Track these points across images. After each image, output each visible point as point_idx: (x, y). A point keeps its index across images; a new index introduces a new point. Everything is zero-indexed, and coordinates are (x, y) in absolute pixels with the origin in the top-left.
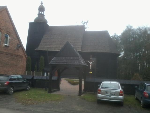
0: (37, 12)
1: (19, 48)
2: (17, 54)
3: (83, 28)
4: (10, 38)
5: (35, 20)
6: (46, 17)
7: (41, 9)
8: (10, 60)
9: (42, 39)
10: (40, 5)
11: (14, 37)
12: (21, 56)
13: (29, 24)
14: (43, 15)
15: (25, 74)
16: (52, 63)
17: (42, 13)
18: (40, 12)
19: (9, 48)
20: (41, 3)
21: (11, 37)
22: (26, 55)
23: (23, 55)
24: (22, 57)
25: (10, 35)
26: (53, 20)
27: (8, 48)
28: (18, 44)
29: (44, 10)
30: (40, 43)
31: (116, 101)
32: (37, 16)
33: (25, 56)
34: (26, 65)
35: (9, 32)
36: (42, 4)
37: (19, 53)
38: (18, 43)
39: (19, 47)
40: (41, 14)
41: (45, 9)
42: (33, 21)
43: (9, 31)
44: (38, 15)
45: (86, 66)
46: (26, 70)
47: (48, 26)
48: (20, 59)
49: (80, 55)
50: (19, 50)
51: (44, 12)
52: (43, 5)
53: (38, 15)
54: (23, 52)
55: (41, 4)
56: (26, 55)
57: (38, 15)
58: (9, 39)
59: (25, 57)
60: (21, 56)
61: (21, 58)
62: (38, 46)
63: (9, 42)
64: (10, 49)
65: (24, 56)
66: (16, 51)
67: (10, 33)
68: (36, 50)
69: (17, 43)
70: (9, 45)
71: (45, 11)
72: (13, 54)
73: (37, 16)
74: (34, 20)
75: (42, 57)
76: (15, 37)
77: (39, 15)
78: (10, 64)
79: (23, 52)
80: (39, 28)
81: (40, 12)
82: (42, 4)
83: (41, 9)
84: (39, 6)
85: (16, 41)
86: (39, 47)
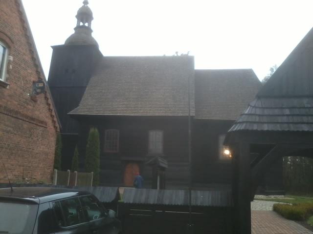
0: (74, 23)
1: (38, 94)
2: (29, 114)
4: (11, 58)
6: (94, 35)
7: (85, 15)
8: (8, 132)
9: (86, 87)
10: (81, 5)
11: (24, 56)
12: (42, 122)
13: (51, 50)
14: (88, 30)
15: (52, 178)
17: (86, 24)
18: (81, 24)
19: (7, 91)
21: (13, 55)
22: (55, 119)
23: (47, 120)
24: (46, 125)
25: (12, 48)
26: (111, 43)
27: (4, 89)
28: (34, 82)
30: (83, 93)
31: (58, 176)
33: (54, 122)
34: (56, 151)
35: (10, 38)
37: (37, 113)
38: (34, 78)
39: (38, 91)
40: (84, 27)
42: (61, 41)
43: (9, 34)
46: (55, 167)
48: (40, 130)
49: (235, 129)
50: (38, 102)
53: (75, 29)
54: (49, 109)
55: (83, 5)
56: (55, 119)
58: (9, 63)
59: (52, 127)
60: (42, 123)
61: (42, 128)
62: (76, 104)
63: (8, 71)
64: (10, 96)
65: (50, 122)
66: (27, 104)
67: (13, 43)
68: (71, 113)
69: (33, 79)
70: (7, 79)
72: (17, 113)
73: (73, 32)
74: (66, 42)
75: (93, 131)
76: (27, 58)
77: (78, 28)
78: (9, 145)
79: (49, 109)
80: (78, 54)
83: (85, 15)
85: (29, 71)
86: (81, 105)
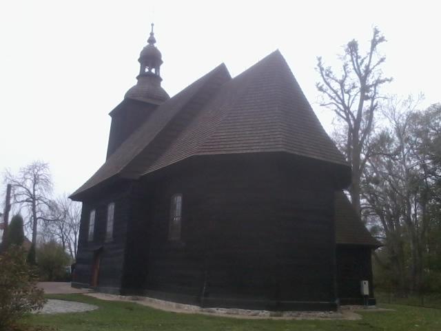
0: (136, 68)
3: (221, 71)
5: (142, 52)
10: (127, 78)
14: (156, 79)
16: (261, 318)
17: (153, 71)
18: (147, 70)
20: (147, 39)
29: (161, 62)
32: (137, 81)
36: (152, 41)
40: (150, 75)
41: (162, 59)
44: (138, 78)
45: (347, 199)
47: (160, 84)
51: (159, 69)
52: (155, 45)
57: (138, 78)
71: (162, 67)
73: (135, 82)
77: (142, 77)
81: (147, 70)
82: (152, 41)
84: (142, 49)
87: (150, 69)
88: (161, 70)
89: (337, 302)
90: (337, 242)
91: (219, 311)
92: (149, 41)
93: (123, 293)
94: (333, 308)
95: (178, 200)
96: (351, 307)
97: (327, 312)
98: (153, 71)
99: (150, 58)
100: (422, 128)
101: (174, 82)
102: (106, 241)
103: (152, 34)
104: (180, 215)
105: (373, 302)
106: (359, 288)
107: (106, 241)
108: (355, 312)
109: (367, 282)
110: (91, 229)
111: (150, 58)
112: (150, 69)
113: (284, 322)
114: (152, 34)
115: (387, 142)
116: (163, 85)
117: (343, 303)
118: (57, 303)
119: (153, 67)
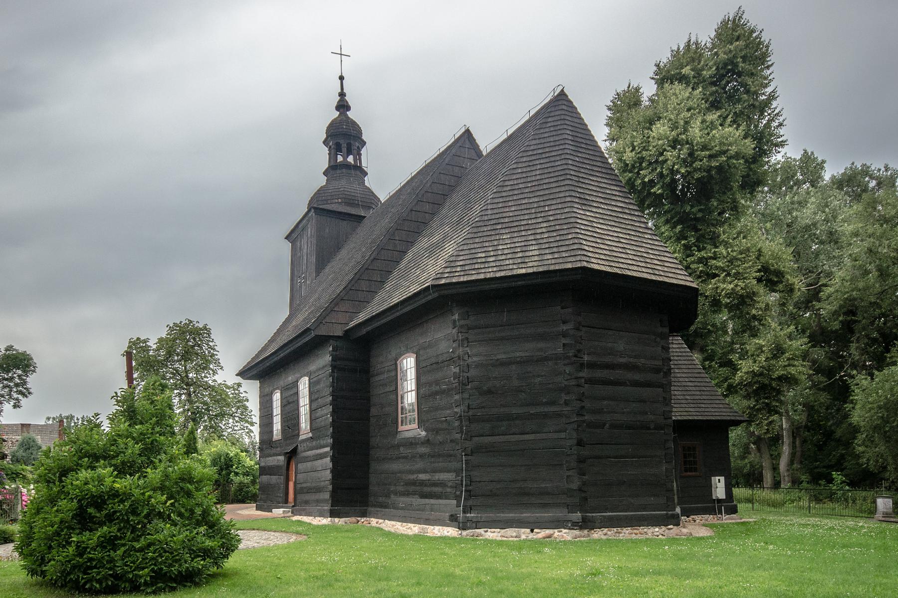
0: (321, 157)
14: (359, 171)
17: (350, 159)
18: (340, 158)
36: (343, 106)
77: (333, 170)
81: (340, 158)
87: (345, 158)
88: (363, 158)
89: (678, 510)
90: (674, 418)
91: (489, 533)
92: (338, 108)
93: (333, 514)
94: (675, 520)
95: (409, 364)
96: (698, 518)
97: (664, 528)
98: (350, 159)
99: (344, 137)
100: (855, 430)
101: (387, 172)
102: (302, 437)
103: (342, 94)
104: (414, 388)
105: (733, 510)
106: (709, 487)
107: (302, 437)
108: (704, 525)
109: (722, 479)
110: (277, 426)
111: (344, 137)
112: (345, 158)
113: (597, 541)
114: (342, 94)
115: (700, 75)
116: (369, 182)
117: (687, 513)
118: (259, 537)
119: (349, 152)
